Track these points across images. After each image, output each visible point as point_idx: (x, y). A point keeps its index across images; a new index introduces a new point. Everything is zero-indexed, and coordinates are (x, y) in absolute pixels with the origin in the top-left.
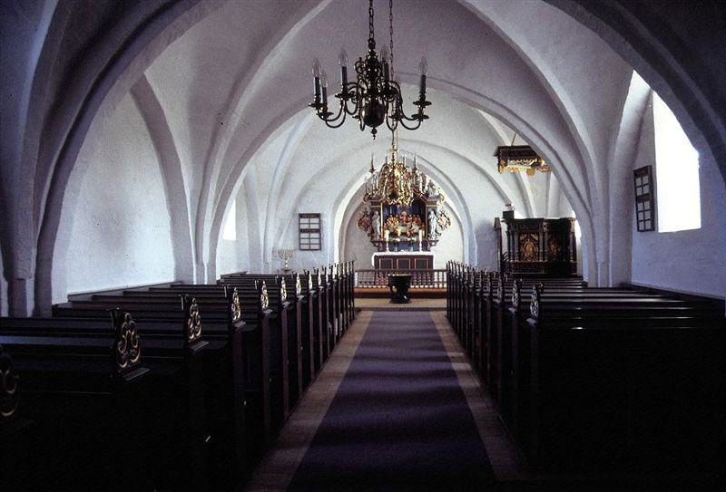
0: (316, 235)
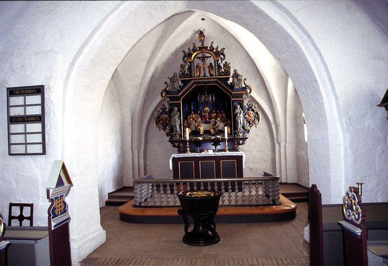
0: (37, 127)
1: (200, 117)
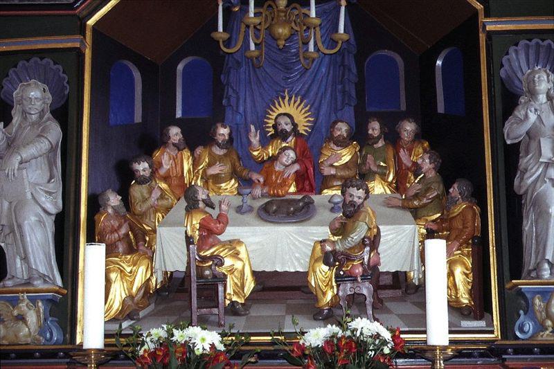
1: (234, 174)
